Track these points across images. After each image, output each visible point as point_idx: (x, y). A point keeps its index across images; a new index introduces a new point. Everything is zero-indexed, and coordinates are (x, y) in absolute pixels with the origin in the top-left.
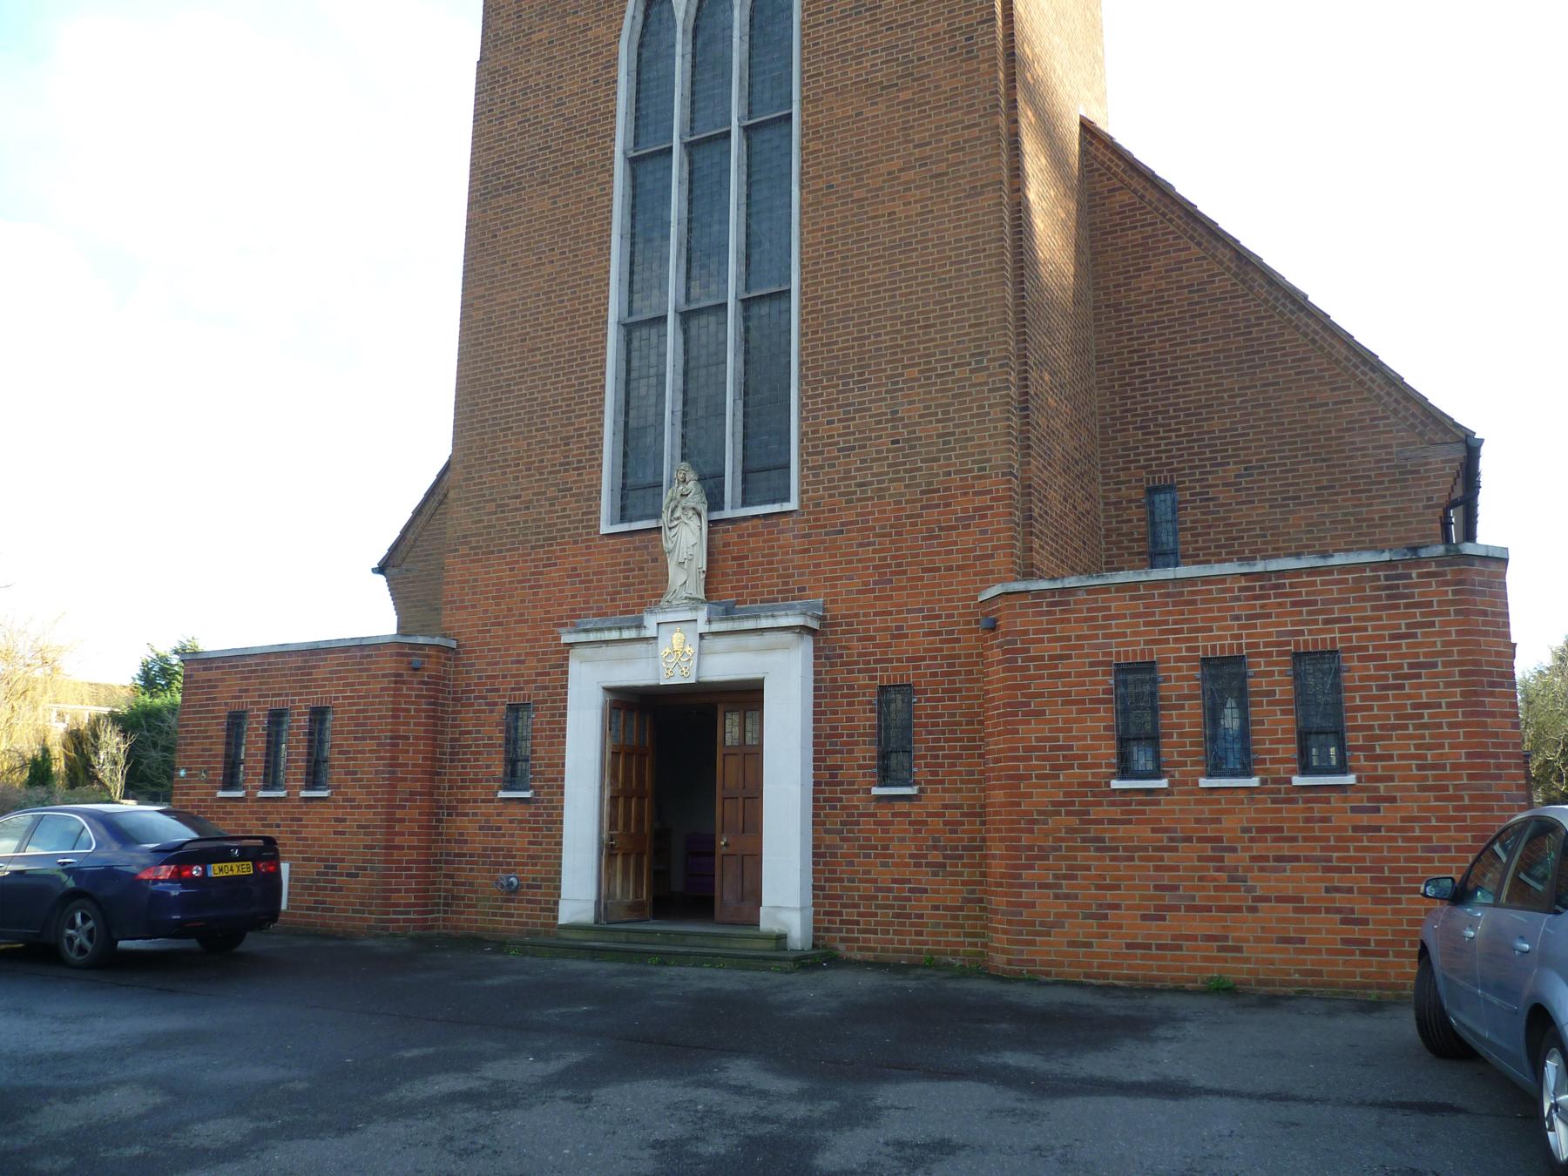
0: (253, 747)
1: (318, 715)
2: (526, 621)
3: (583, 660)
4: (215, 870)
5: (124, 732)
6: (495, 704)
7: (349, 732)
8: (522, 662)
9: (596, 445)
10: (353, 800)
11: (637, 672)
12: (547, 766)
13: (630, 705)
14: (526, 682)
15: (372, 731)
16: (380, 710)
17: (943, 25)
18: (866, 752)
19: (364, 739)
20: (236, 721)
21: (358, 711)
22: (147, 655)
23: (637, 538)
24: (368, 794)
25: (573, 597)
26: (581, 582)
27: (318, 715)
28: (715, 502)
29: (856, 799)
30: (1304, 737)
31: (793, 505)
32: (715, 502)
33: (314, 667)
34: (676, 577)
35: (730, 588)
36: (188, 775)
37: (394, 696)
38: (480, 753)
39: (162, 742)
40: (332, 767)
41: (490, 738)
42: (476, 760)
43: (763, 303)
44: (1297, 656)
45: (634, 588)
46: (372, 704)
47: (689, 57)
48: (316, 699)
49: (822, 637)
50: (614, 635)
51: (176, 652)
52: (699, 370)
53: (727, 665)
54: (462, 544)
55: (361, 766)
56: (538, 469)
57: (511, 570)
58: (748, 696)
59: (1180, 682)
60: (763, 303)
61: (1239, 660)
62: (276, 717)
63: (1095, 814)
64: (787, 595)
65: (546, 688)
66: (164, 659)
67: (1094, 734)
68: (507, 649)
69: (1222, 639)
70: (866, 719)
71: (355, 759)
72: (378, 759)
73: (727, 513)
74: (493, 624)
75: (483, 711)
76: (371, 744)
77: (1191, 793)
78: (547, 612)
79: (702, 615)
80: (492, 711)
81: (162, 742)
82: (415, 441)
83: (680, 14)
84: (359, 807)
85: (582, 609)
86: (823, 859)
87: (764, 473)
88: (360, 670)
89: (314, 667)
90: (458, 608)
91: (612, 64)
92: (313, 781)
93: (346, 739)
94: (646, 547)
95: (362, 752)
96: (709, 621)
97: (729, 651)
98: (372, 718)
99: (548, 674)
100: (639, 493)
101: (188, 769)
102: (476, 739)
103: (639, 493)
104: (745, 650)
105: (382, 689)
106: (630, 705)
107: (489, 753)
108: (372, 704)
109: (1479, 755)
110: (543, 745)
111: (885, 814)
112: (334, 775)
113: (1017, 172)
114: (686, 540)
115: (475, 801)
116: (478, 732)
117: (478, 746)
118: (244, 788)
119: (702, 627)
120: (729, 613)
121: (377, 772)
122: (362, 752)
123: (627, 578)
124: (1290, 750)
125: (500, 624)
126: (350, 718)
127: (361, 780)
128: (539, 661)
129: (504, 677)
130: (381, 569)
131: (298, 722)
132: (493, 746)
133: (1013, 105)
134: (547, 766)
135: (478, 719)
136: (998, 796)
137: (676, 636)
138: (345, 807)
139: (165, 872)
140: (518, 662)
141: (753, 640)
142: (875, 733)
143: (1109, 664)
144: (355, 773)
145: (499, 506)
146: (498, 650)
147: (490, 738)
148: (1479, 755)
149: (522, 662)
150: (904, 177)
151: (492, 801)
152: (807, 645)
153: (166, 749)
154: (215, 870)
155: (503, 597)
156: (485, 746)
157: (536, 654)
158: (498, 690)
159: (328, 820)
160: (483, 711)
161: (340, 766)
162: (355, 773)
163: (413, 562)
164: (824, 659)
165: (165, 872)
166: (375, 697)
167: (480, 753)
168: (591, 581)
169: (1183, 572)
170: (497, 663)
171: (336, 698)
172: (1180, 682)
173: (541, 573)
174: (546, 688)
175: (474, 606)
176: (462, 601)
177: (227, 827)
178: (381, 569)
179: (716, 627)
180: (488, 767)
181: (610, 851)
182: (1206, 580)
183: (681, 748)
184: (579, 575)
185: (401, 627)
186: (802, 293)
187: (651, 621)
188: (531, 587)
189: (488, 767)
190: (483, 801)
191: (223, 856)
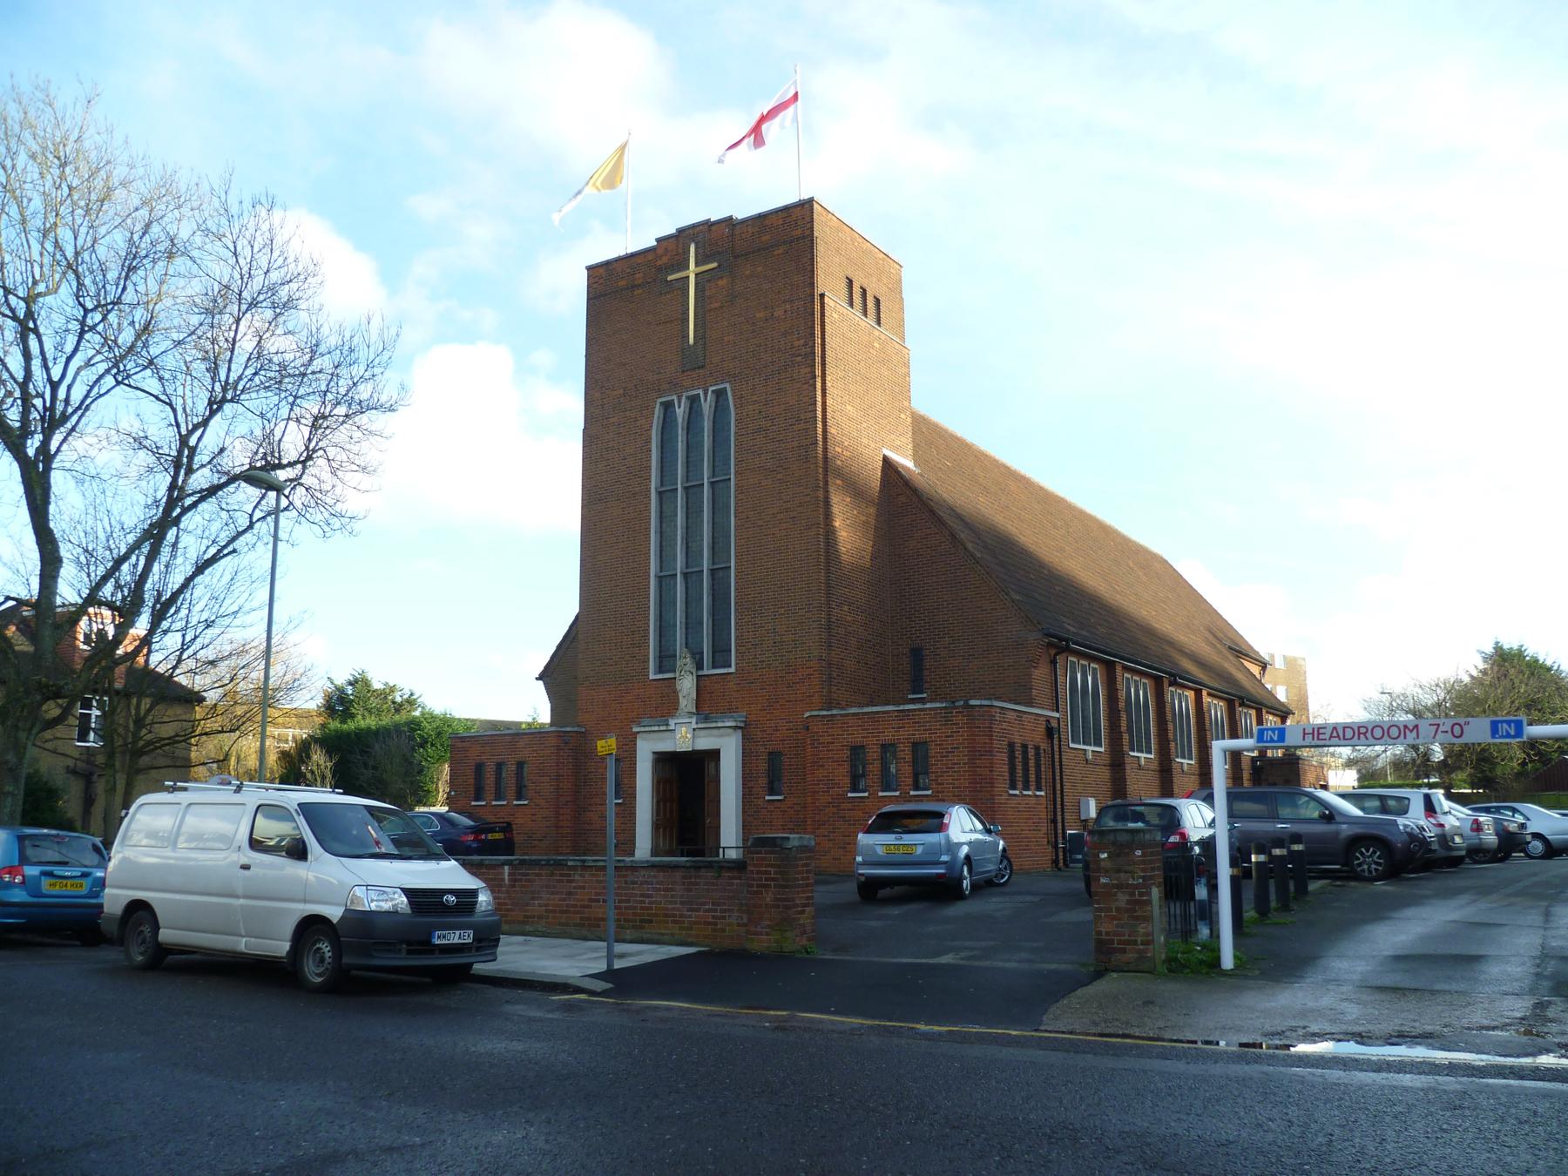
0: (489, 779)
1: (520, 765)
4: (490, 836)
5: (329, 753)
9: (647, 636)
11: (666, 746)
13: (664, 760)
17: (796, 444)
18: (763, 781)
20: (479, 768)
22: (330, 688)
27: (520, 765)
28: (700, 666)
29: (760, 802)
30: (916, 776)
31: (732, 670)
32: (700, 666)
34: (683, 702)
35: (706, 709)
36: (1144, 855)
39: (371, 763)
43: (719, 574)
44: (883, 746)
45: (663, 707)
49: (746, 730)
51: (350, 684)
52: (692, 601)
53: (705, 743)
58: (714, 755)
59: (873, 753)
60: (719, 574)
61: (893, 745)
62: (499, 766)
63: (843, 806)
64: (730, 710)
66: (341, 690)
67: (842, 774)
69: (888, 736)
70: (763, 766)
73: (705, 672)
79: (694, 720)
81: (371, 763)
82: (556, 604)
83: (680, 420)
86: (747, 827)
87: (720, 654)
91: (649, 441)
100: (666, 660)
103: (666, 660)
106: (664, 760)
111: (771, 807)
113: (828, 516)
114: (687, 685)
120: (707, 719)
124: (910, 781)
130: (539, 678)
133: (826, 483)
136: (809, 800)
139: (471, 837)
142: (766, 771)
150: (780, 516)
152: (739, 733)
153: (375, 768)
154: (490, 836)
163: (558, 675)
164: (746, 739)
165: (471, 837)
172: (873, 753)
177: (491, 819)
178: (539, 678)
181: (657, 826)
183: (687, 777)
187: (672, 722)
191: (492, 830)
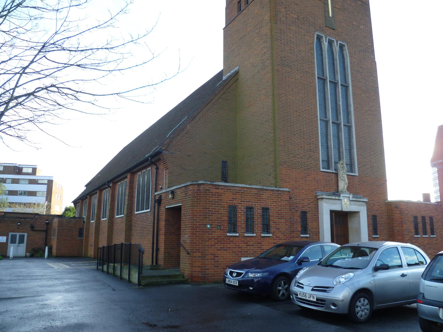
0: (241, 218)
3: (326, 203)
6: (298, 211)
7: (276, 216)
10: (279, 237)
11: (337, 207)
12: (312, 228)
15: (283, 217)
16: (285, 211)
19: (281, 219)
21: (278, 210)
23: (328, 174)
27: (265, 210)
33: (262, 194)
36: (211, 227)
37: (192, 202)
40: (272, 227)
41: (297, 220)
46: (283, 208)
47: (324, 58)
48: (263, 205)
50: (334, 198)
54: (284, 164)
55: (281, 227)
56: (304, 149)
57: (299, 174)
65: (310, 208)
71: (279, 225)
72: (286, 225)
75: (294, 212)
77: (243, 237)
89: (262, 194)
90: (285, 182)
92: (433, 233)
93: (275, 218)
95: (281, 223)
97: (354, 205)
98: (284, 213)
101: (210, 225)
104: (356, 205)
105: (286, 204)
108: (283, 208)
112: (272, 229)
115: (294, 237)
116: (293, 218)
117: (293, 222)
118: (238, 233)
119: (351, 199)
121: (286, 229)
122: (281, 223)
125: (297, 189)
126: (276, 212)
127: (281, 231)
128: (308, 200)
131: (258, 212)
132: (298, 222)
134: (312, 228)
135: (293, 214)
138: (276, 239)
140: (303, 200)
143: (244, 206)
144: (279, 229)
145: (294, 156)
147: (297, 220)
151: (298, 237)
156: (295, 222)
157: (307, 198)
158: (298, 207)
160: (294, 212)
162: (279, 229)
166: (283, 206)
169: (237, 185)
171: (271, 205)
174: (310, 208)
175: (289, 182)
176: (286, 180)
179: (354, 199)
180: (297, 228)
182: (250, 188)
186: (317, 120)
188: (304, 180)
189: (297, 228)
190: (296, 237)
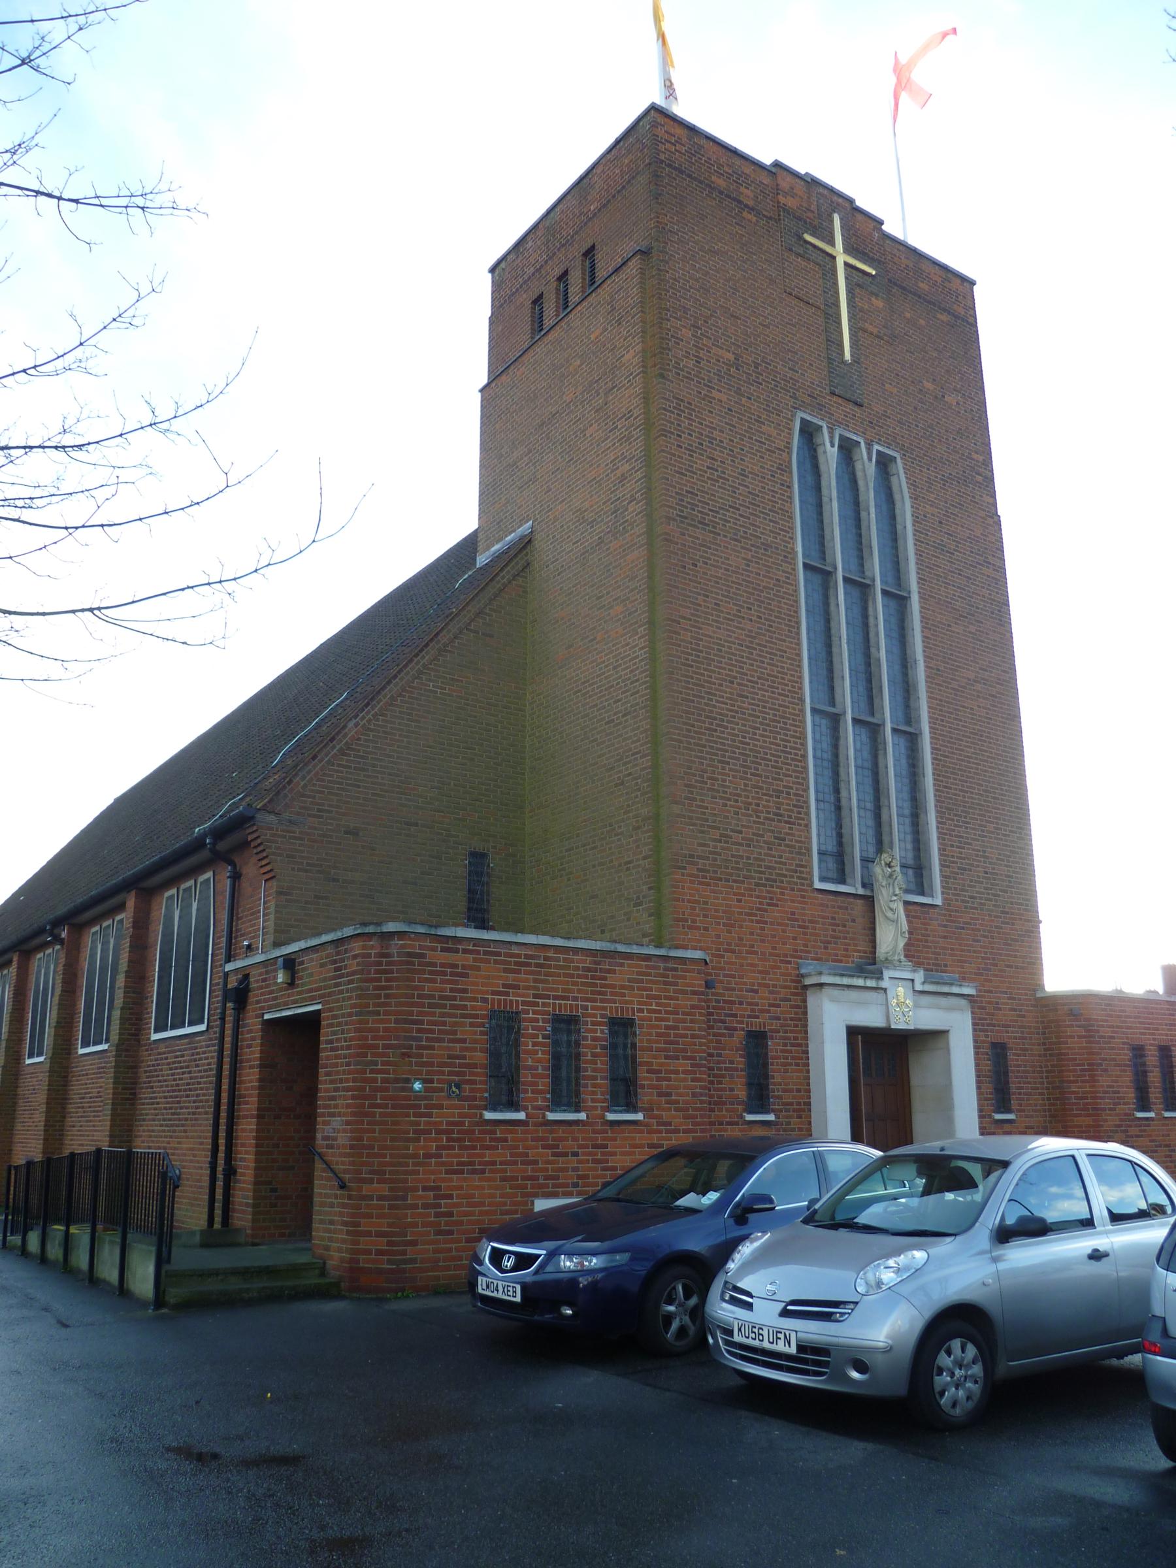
0: (535, 1056)
1: (621, 1027)
2: (756, 953)
3: (832, 1000)
6: (735, 1029)
7: (659, 1050)
8: (756, 992)
10: (670, 1124)
11: (870, 1017)
12: (785, 1091)
14: (762, 1011)
23: (840, 898)
24: (685, 1117)
25: (795, 938)
26: (800, 927)
27: (621, 1027)
38: (723, 1076)
41: (732, 1062)
42: (720, 1083)
48: (615, 1008)
50: (860, 982)
55: (677, 1088)
65: (778, 1018)
68: (741, 977)
71: (669, 1080)
74: (726, 951)
76: (683, 1064)
78: (774, 948)
80: (731, 1036)
84: (676, 1131)
85: (802, 951)
88: (665, 983)
89: (609, 971)
90: (690, 927)
93: (655, 1057)
94: (846, 908)
95: (677, 1072)
96: (924, 983)
98: (685, 1036)
99: (778, 1006)
101: (425, 1081)
102: (718, 1062)
104: (938, 1007)
107: (731, 1076)
109: (406, 1021)
110: (779, 1071)
112: (645, 1096)
115: (721, 1124)
116: (719, 1055)
117: (720, 1069)
118: (525, 1109)
122: (677, 1072)
123: (834, 931)
125: (733, 952)
126: (658, 1035)
127: (677, 1102)
129: (741, 1003)
132: (736, 1069)
137: (901, 989)
138: (660, 1132)
141: (943, 1001)
144: (670, 1095)
146: (733, 976)
147: (732, 1062)
148: (406, 1021)
149: (756, 992)
151: (736, 1124)
155: (733, 926)
156: (726, 1069)
157: (767, 986)
158: (735, 1016)
159: (642, 1146)
161: (651, 1087)
162: (670, 1095)
167: (723, 1076)
168: (807, 928)
170: (734, 989)
173: (766, 910)
174: (778, 1018)
176: (694, 921)
179: (928, 988)
180: (732, 1090)
184: (797, 920)
185: (1077, 1010)
188: (758, 922)
189: (732, 1090)
190: (729, 1123)
